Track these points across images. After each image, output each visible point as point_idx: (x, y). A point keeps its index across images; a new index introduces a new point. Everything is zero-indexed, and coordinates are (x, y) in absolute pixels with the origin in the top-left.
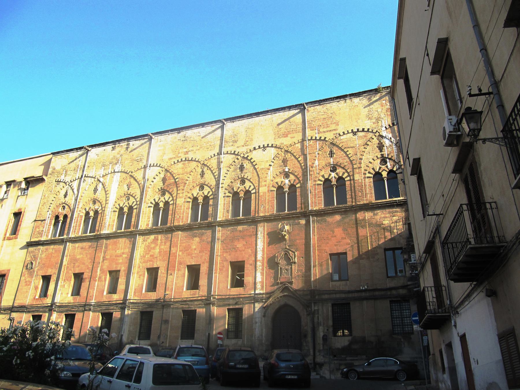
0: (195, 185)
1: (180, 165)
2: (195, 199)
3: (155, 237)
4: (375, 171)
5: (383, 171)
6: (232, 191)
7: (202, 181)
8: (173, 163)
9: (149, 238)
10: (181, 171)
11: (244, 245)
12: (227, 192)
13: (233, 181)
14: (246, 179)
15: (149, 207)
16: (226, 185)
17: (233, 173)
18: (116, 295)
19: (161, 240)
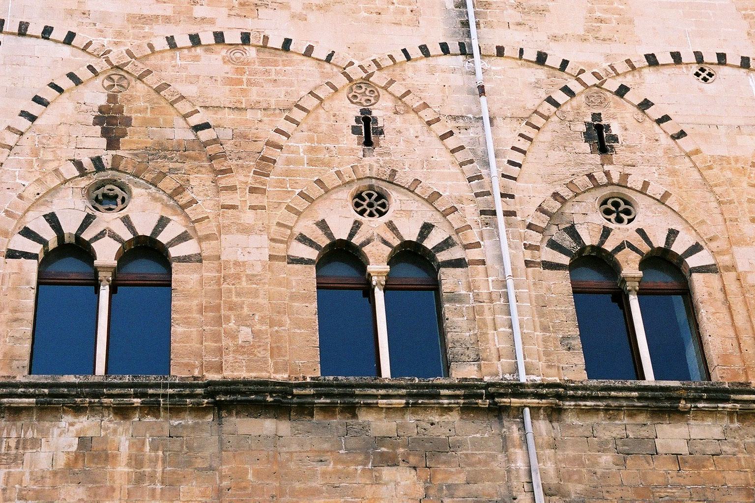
0: (331, 180)
1: (213, 62)
2: (342, 254)
3: (84, 442)
4: (329, 235)
5: (101, 235)
6: (568, 242)
7: (373, 164)
8: (161, 44)
9: (35, 443)
10: (221, 94)
11: (598, 464)
12: (535, 238)
13: (565, 193)
14: (643, 192)
15: (12, 254)
16: (532, 208)
17: (556, 155)
18: (28, 226)
19: (136, 461)
